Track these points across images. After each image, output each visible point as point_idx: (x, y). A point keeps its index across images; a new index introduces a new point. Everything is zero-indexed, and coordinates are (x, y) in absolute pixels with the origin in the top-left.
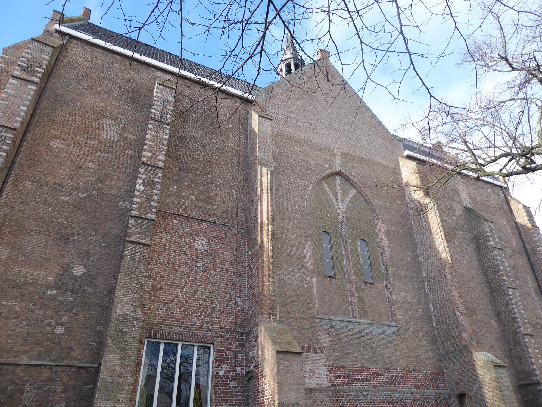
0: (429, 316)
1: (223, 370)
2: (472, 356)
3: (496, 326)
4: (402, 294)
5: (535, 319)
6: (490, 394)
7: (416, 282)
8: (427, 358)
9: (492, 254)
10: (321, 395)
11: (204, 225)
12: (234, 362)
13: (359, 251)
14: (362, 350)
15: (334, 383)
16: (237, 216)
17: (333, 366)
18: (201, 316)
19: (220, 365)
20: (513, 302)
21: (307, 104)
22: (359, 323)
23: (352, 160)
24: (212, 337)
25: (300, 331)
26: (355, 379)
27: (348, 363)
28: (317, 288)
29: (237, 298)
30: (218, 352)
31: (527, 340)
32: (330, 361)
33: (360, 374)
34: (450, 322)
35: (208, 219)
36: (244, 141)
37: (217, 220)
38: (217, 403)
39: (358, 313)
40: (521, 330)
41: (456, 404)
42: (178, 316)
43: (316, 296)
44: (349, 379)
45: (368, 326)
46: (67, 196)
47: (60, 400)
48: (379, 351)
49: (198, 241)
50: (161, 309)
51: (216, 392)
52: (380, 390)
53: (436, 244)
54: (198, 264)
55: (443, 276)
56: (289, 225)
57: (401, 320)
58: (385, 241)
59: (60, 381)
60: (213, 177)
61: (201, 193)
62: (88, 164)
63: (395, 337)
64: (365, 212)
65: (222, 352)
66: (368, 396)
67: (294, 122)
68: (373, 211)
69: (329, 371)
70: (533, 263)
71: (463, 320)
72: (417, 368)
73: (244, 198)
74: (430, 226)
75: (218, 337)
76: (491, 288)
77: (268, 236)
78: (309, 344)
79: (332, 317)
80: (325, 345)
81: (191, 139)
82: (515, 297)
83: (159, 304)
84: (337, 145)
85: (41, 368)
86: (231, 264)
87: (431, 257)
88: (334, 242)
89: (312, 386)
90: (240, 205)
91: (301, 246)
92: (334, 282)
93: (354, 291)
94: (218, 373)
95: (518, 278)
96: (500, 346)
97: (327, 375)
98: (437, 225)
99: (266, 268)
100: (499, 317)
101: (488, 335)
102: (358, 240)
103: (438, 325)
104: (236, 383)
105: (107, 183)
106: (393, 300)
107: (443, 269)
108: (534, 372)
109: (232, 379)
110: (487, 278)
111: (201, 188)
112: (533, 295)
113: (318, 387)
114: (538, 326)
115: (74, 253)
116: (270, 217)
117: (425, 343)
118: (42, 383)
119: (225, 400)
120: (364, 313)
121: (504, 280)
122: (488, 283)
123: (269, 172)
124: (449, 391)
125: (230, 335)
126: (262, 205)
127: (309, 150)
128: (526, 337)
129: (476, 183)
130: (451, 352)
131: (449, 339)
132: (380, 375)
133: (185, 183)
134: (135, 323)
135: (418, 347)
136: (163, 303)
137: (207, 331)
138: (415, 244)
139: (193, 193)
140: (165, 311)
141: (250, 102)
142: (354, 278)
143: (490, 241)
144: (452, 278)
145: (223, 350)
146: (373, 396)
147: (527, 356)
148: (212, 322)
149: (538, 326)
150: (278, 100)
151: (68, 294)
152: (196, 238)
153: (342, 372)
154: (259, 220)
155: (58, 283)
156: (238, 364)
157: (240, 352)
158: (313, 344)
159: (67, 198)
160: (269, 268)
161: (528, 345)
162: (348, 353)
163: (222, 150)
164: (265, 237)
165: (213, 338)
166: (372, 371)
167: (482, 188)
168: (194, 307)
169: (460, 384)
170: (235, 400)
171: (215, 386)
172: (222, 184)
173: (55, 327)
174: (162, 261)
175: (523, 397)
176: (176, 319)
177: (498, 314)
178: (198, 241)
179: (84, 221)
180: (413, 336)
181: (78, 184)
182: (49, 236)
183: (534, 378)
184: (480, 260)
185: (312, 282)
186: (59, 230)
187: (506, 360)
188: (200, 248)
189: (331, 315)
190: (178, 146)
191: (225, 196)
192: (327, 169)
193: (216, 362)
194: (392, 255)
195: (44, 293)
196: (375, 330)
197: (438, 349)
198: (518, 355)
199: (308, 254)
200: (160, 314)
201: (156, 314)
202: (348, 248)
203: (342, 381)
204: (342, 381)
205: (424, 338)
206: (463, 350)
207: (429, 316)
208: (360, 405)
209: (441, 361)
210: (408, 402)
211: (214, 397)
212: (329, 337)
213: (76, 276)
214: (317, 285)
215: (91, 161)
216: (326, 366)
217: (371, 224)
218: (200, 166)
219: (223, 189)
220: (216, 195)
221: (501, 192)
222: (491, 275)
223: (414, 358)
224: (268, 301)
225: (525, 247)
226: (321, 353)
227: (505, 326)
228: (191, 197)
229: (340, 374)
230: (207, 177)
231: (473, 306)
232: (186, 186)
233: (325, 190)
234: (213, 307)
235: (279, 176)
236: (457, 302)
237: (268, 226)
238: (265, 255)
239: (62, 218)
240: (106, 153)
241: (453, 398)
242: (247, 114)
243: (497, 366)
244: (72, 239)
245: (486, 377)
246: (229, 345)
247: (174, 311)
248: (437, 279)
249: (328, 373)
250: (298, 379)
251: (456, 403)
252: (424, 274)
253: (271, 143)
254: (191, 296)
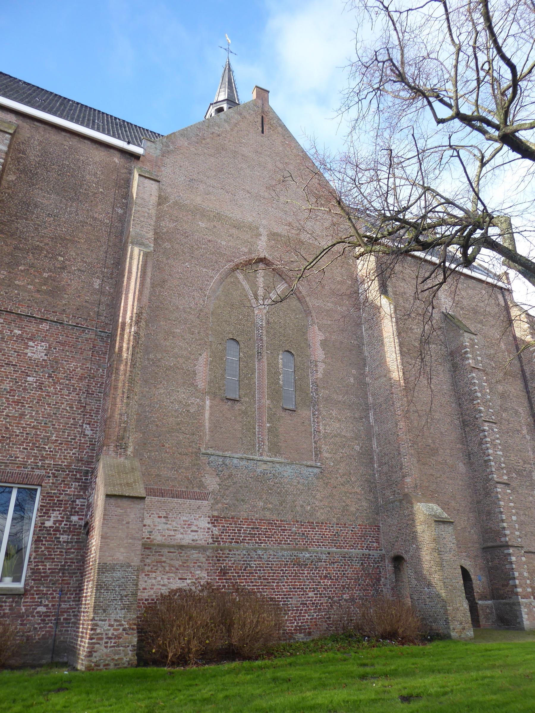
0: (369, 455)
1: (52, 519)
2: (412, 507)
3: (464, 471)
4: (334, 425)
5: (521, 464)
6: (428, 558)
7: (358, 409)
9: (469, 376)
10: (195, 554)
11: (45, 326)
12: (69, 509)
13: (280, 366)
14: (264, 496)
16: (98, 314)
18: (27, 449)
19: (48, 513)
20: (488, 439)
21: (226, 163)
22: (265, 462)
24: (39, 476)
25: (176, 470)
26: (249, 534)
28: (211, 414)
29: (84, 426)
30: (47, 496)
31: (499, 490)
32: (215, 510)
33: (257, 528)
35: (52, 318)
36: (120, 211)
37: (66, 319)
38: (38, 562)
39: (266, 449)
40: (493, 477)
41: (390, 568)
43: (207, 424)
45: (278, 466)
48: (289, 498)
49: (33, 347)
51: (38, 548)
52: (282, 549)
53: (388, 359)
54: (29, 379)
55: (391, 402)
56: (176, 328)
57: (327, 459)
58: (319, 354)
61: (45, 282)
63: (315, 481)
64: (296, 315)
66: (265, 556)
67: (202, 187)
68: (308, 313)
69: (212, 523)
70: (531, 391)
71: (409, 462)
72: (342, 522)
73: (112, 291)
74: (382, 336)
75: (49, 477)
76: (464, 422)
78: (187, 487)
79: (227, 454)
80: (211, 490)
81: (36, 206)
82: (492, 434)
84: (264, 222)
86: (81, 379)
87: (380, 377)
88: (244, 353)
89: (184, 543)
90: (103, 299)
91: (192, 357)
92: (237, 406)
93: (265, 419)
94: (44, 523)
95: (505, 410)
96: (465, 496)
97: (209, 529)
98: (391, 334)
99: (120, 385)
100: (470, 459)
101: (451, 481)
102: (281, 352)
103: (379, 467)
104: (70, 537)
106: (320, 432)
107: (392, 393)
108: (503, 532)
110: (461, 408)
111: (46, 275)
112: (525, 432)
113: (194, 543)
114: (525, 473)
116: (134, 315)
117: (359, 490)
119: (50, 559)
120: (275, 449)
121: (480, 412)
122: (462, 414)
123: (142, 254)
124: (383, 552)
125: (68, 475)
126: (127, 299)
127: (220, 227)
128: (499, 486)
129: (466, 281)
130: (388, 500)
131: (390, 485)
132: (287, 530)
133: (21, 268)
135: (348, 495)
137: (33, 468)
138: (364, 359)
139: (32, 281)
141: (136, 157)
142: (268, 402)
143: (468, 358)
144: (402, 405)
145: (54, 493)
146: (272, 557)
147: (497, 510)
148: (42, 456)
149: (525, 473)
150: (181, 156)
152: (31, 343)
154: (120, 320)
157: (79, 497)
158: (193, 488)
161: (500, 496)
162: (243, 500)
163: (84, 223)
164: (125, 344)
165: (41, 478)
167: (474, 289)
168: (18, 436)
170: (65, 559)
171: (36, 541)
172: (79, 270)
175: (488, 562)
177: (469, 455)
178: (33, 347)
180: (342, 480)
183: (503, 539)
184: (455, 384)
185: (203, 407)
187: (471, 515)
188: (35, 356)
189: (226, 451)
190: (16, 215)
191: (80, 285)
193: (42, 510)
194: (326, 373)
196: (288, 471)
197: (377, 499)
198: (486, 509)
199: (201, 369)
202: (263, 362)
204: (229, 536)
205: (358, 483)
206: (403, 500)
207: (369, 455)
208: (250, 567)
209: (377, 514)
210: (322, 565)
211: (34, 554)
212: (218, 479)
214: (211, 410)
216: (209, 517)
217: (303, 331)
218: (48, 244)
219: (79, 277)
220: (69, 285)
221: (500, 297)
222: (465, 403)
223: (339, 509)
224: (117, 429)
225: (523, 371)
226: (204, 500)
227: (475, 471)
228: (29, 287)
229: (228, 527)
231: (434, 443)
232: (22, 271)
233: (239, 282)
234: (46, 436)
235: (169, 261)
236: (404, 437)
237: (131, 328)
238: (122, 367)
241: (387, 561)
242: (130, 174)
243: (440, 522)
245: (425, 535)
248: (384, 406)
249: (210, 526)
250: (134, 532)
251: (390, 567)
252: (371, 399)
253: (154, 214)
254: (13, 421)
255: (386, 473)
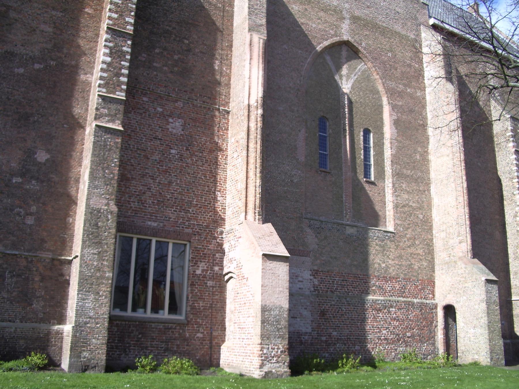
1: (200, 269)
8: (419, 268)
12: (211, 261)
15: (317, 287)
17: (318, 271)
18: (176, 211)
23: (364, 25)
27: (335, 268)
33: (346, 281)
34: (451, 231)
42: (152, 210)
44: (333, 284)
46: (22, 67)
47: (39, 289)
49: (172, 123)
50: (132, 202)
54: (173, 151)
59: (36, 271)
60: (190, 43)
62: (43, 27)
65: (199, 251)
69: (313, 275)
75: (195, 235)
77: (257, 122)
83: (130, 196)
85: (17, 257)
97: (311, 280)
104: (214, 283)
105: (65, 51)
109: (209, 278)
111: (176, 57)
115: (36, 136)
118: (20, 272)
133: (157, 51)
134: (109, 216)
136: (134, 194)
140: (136, 204)
145: (200, 248)
151: (33, 182)
152: (171, 120)
153: (327, 277)
155: (22, 170)
156: (216, 263)
159: (21, 71)
160: (256, 160)
166: (359, 277)
168: (168, 200)
169: (448, 296)
171: (191, 285)
172: (201, 52)
173: (24, 217)
174: (131, 147)
176: (149, 212)
178: (172, 123)
179: (43, 98)
180: (408, 243)
181: (32, 52)
182: (8, 116)
186: (17, 108)
188: (174, 131)
192: (333, 36)
195: (10, 180)
198: (514, 269)
200: (131, 207)
201: (127, 207)
203: (326, 286)
204: (326, 286)
212: (316, 240)
213: (40, 163)
215: (45, 23)
216: (311, 270)
220: (194, 66)
229: (325, 279)
230: (183, 43)
232: (158, 54)
234: (189, 201)
239: (19, 95)
240: (61, 12)
244: (32, 119)
246: (207, 244)
247: (147, 204)
249: (312, 277)
254: (164, 188)
255: (444, 239)
